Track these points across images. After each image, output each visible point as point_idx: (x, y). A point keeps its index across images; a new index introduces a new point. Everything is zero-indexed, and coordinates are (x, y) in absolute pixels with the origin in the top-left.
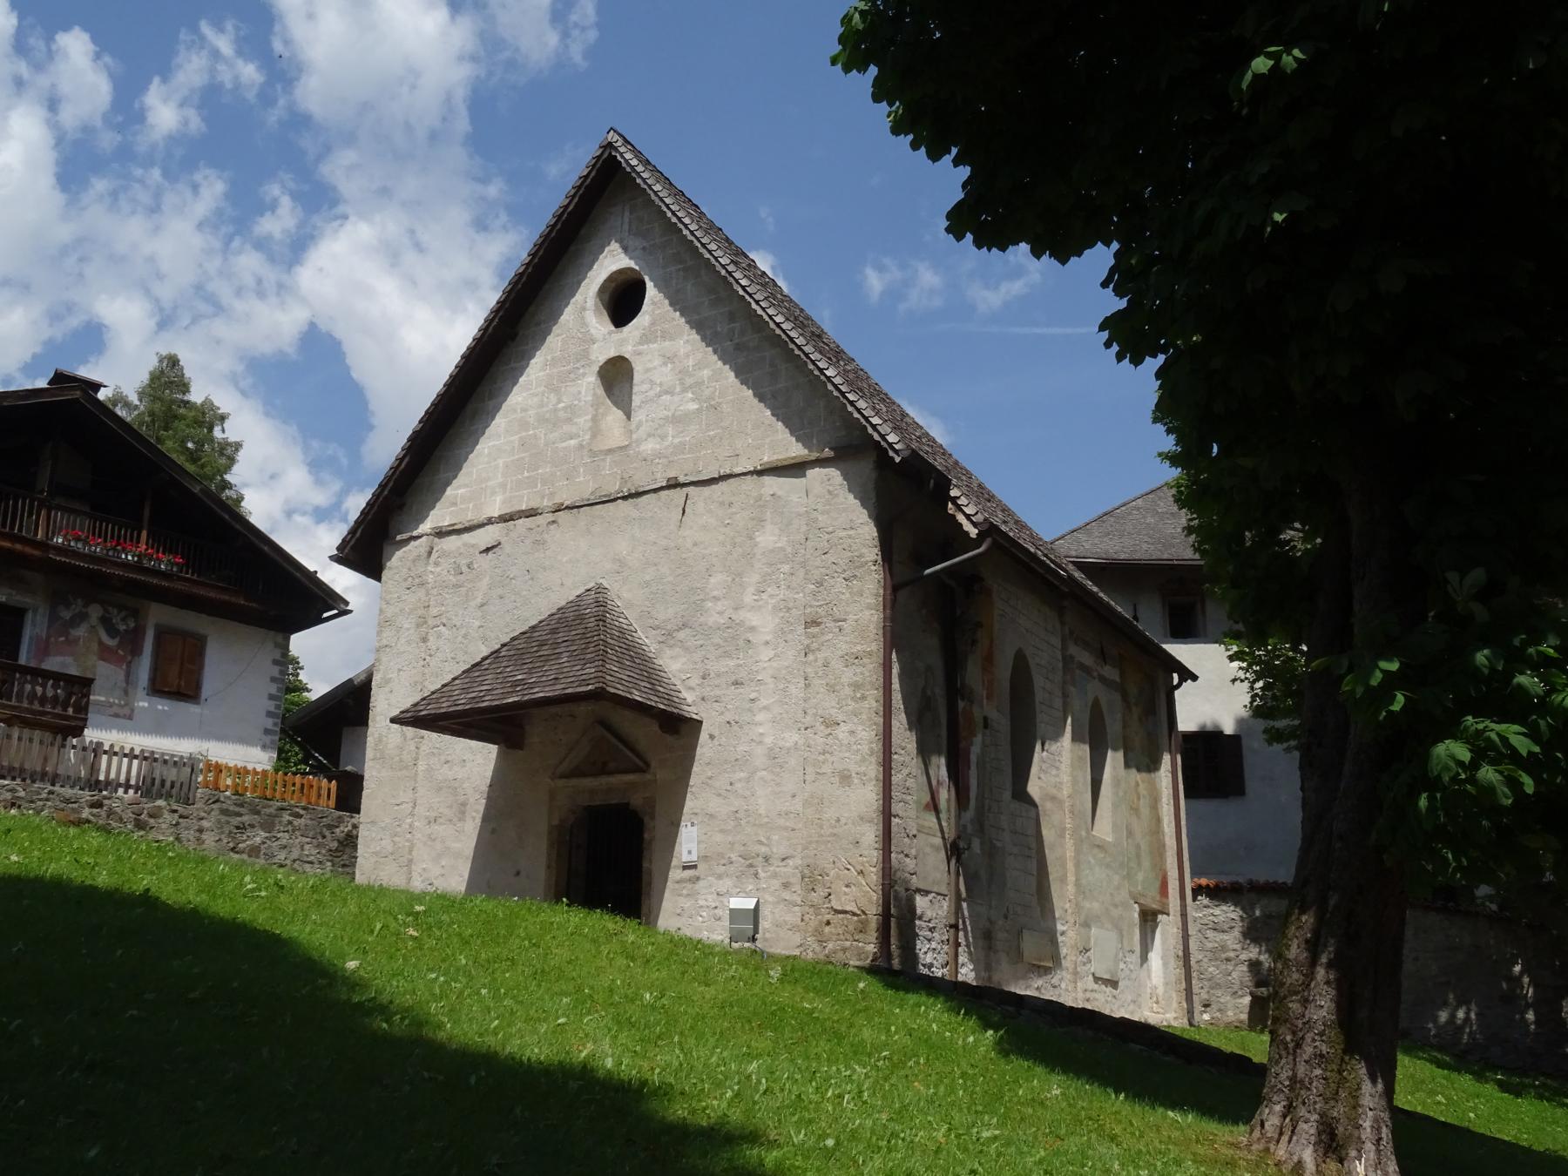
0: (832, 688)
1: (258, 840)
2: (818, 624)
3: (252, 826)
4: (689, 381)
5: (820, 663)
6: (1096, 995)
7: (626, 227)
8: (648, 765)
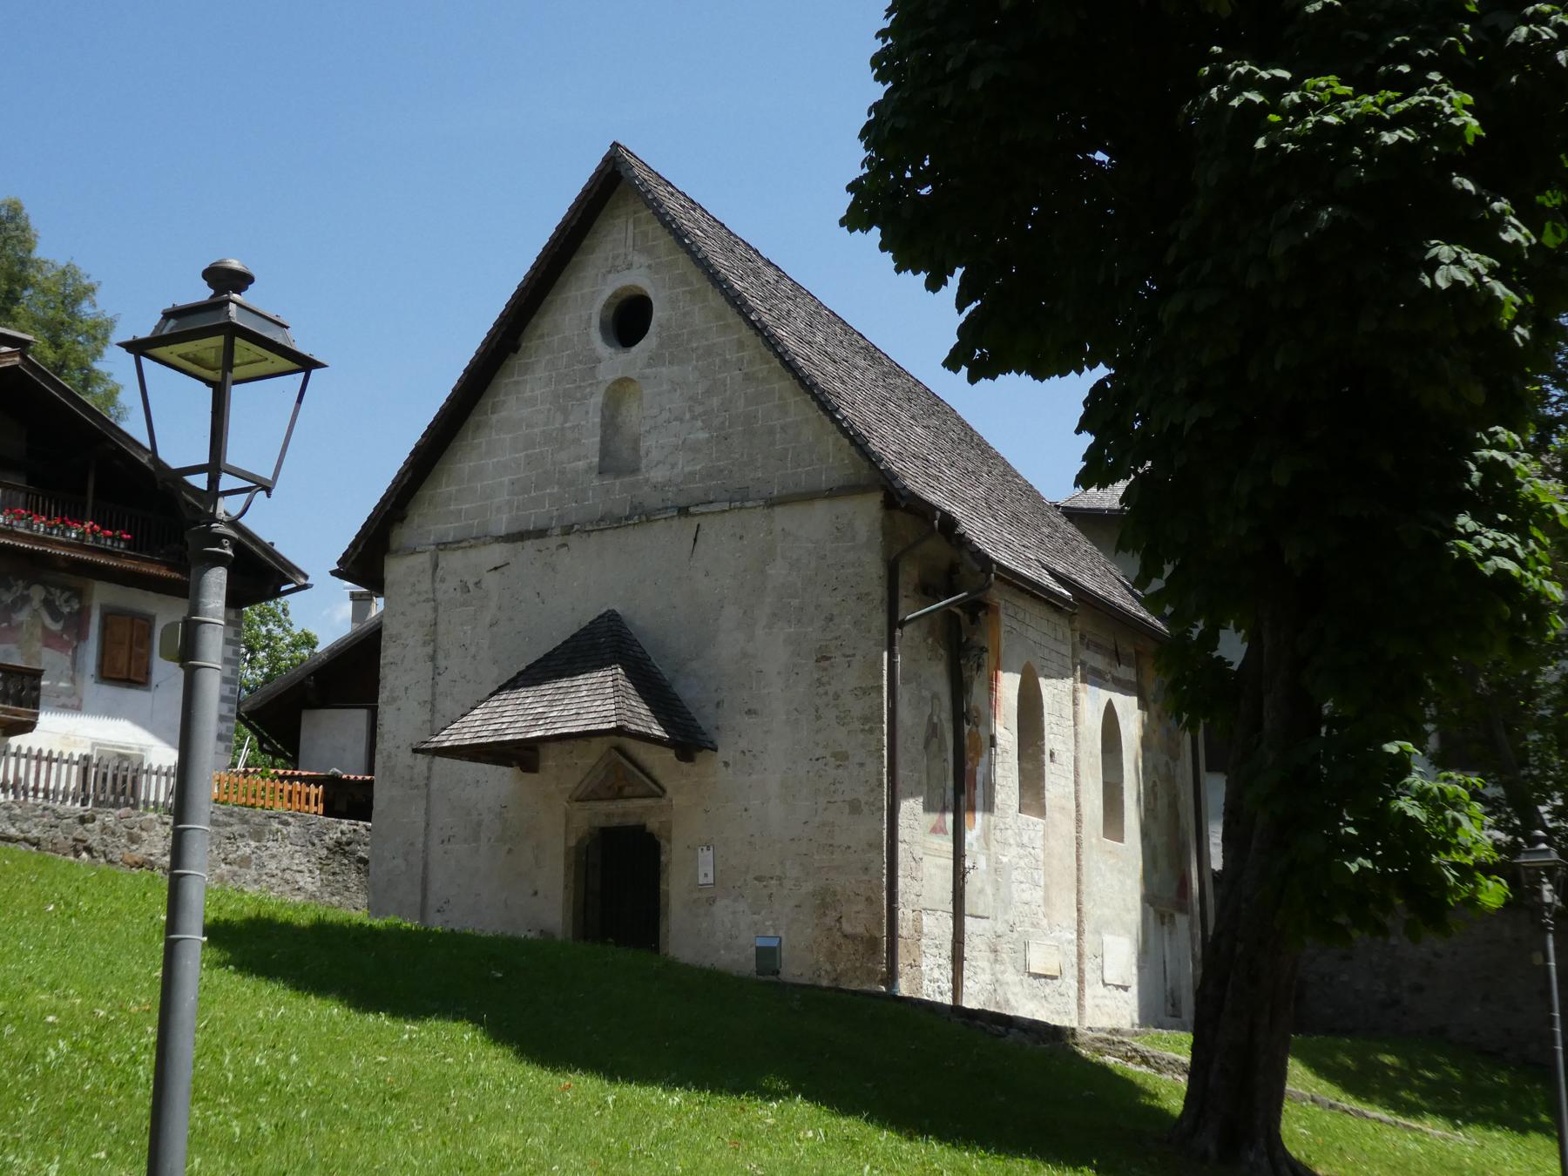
1: (248, 850)
3: (242, 836)
4: (699, 409)
5: (831, 694)
6: (1107, 1002)
7: (629, 242)
8: (664, 791)
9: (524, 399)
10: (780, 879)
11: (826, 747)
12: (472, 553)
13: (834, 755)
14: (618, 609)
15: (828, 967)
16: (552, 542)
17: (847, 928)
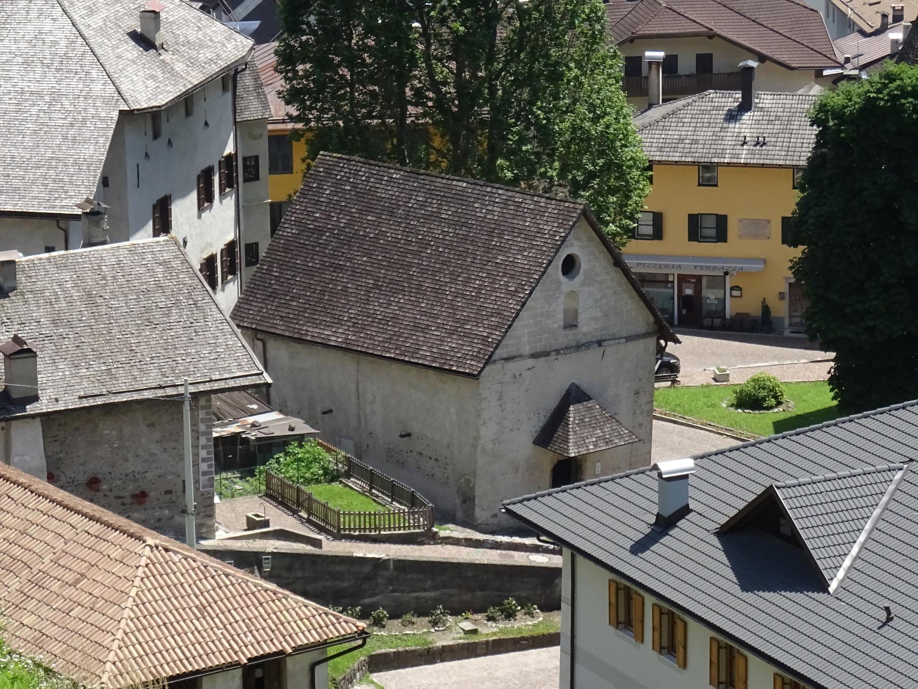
14: (576, 382)
16: (553, 356)
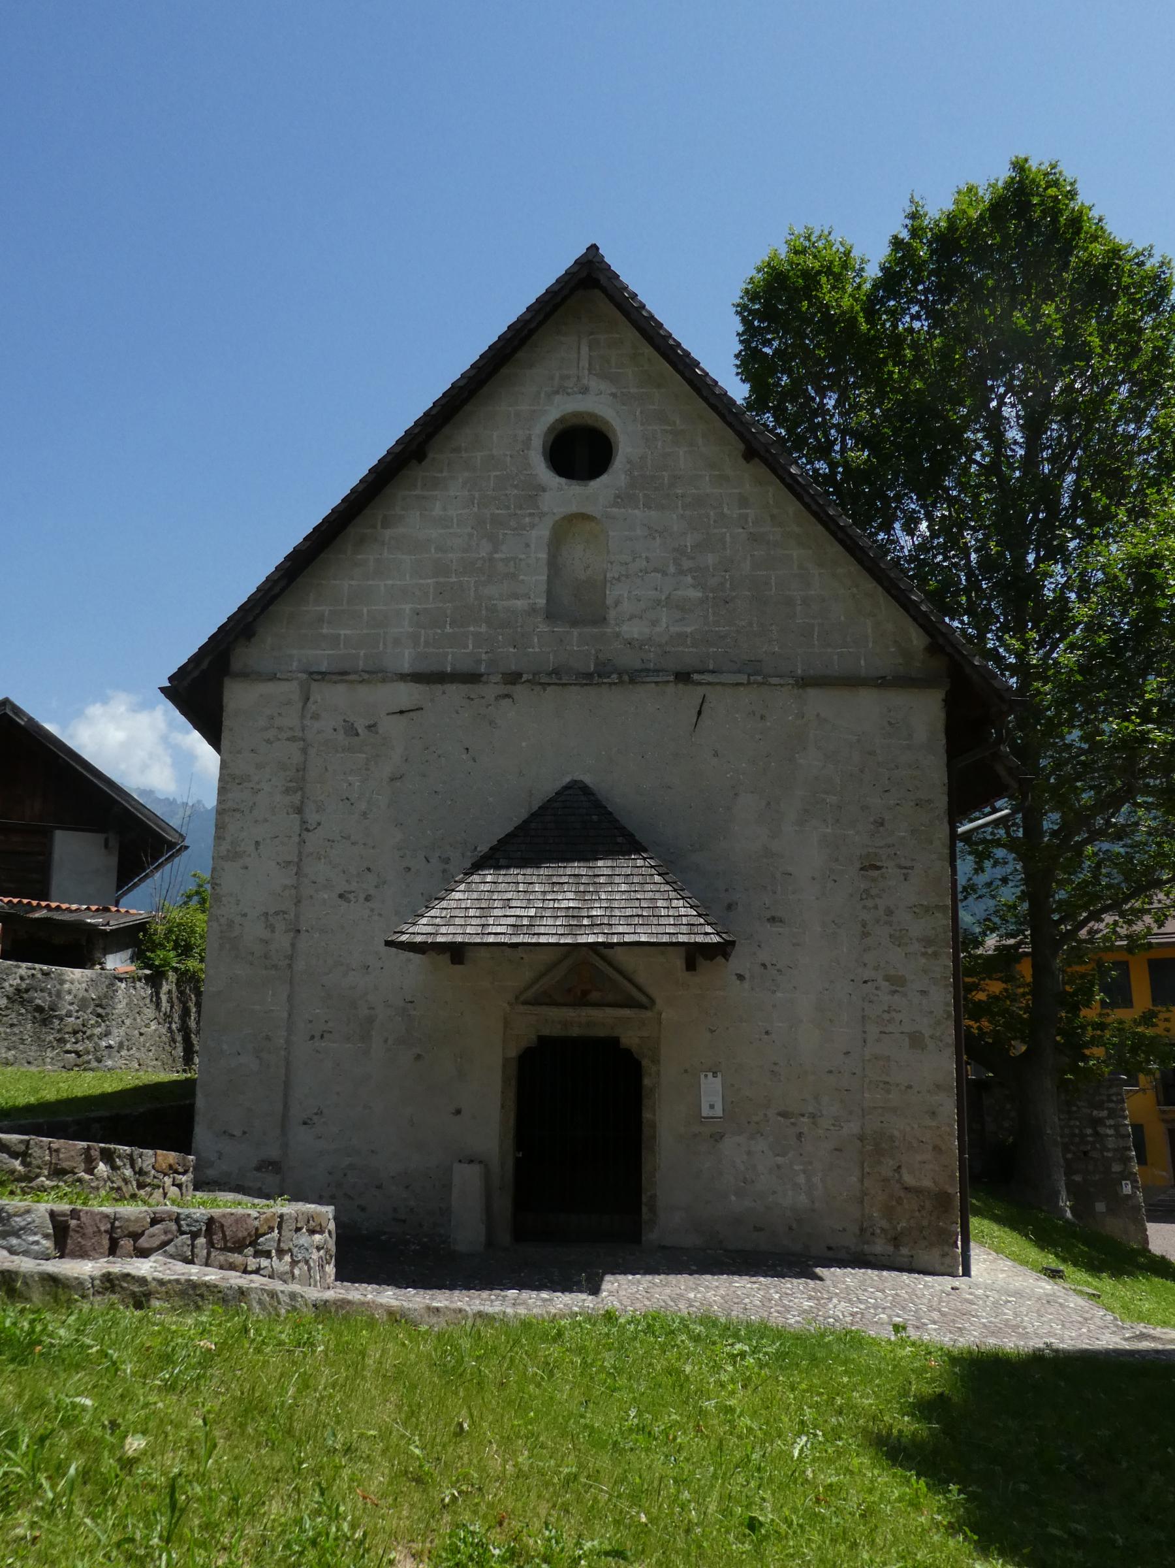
0: (898, 939)
2: (878, 868)
4: (687, 564)
7: (585, 363)
8: (652, 1001)
9: (437, 522)
10: (813, 1116)
11: (876, 968)
12: (363, 692)
13: (887, 978)
14: (587, 779)
15: (884, 1224)
16: (490, 691)
17: (908, 1179)
